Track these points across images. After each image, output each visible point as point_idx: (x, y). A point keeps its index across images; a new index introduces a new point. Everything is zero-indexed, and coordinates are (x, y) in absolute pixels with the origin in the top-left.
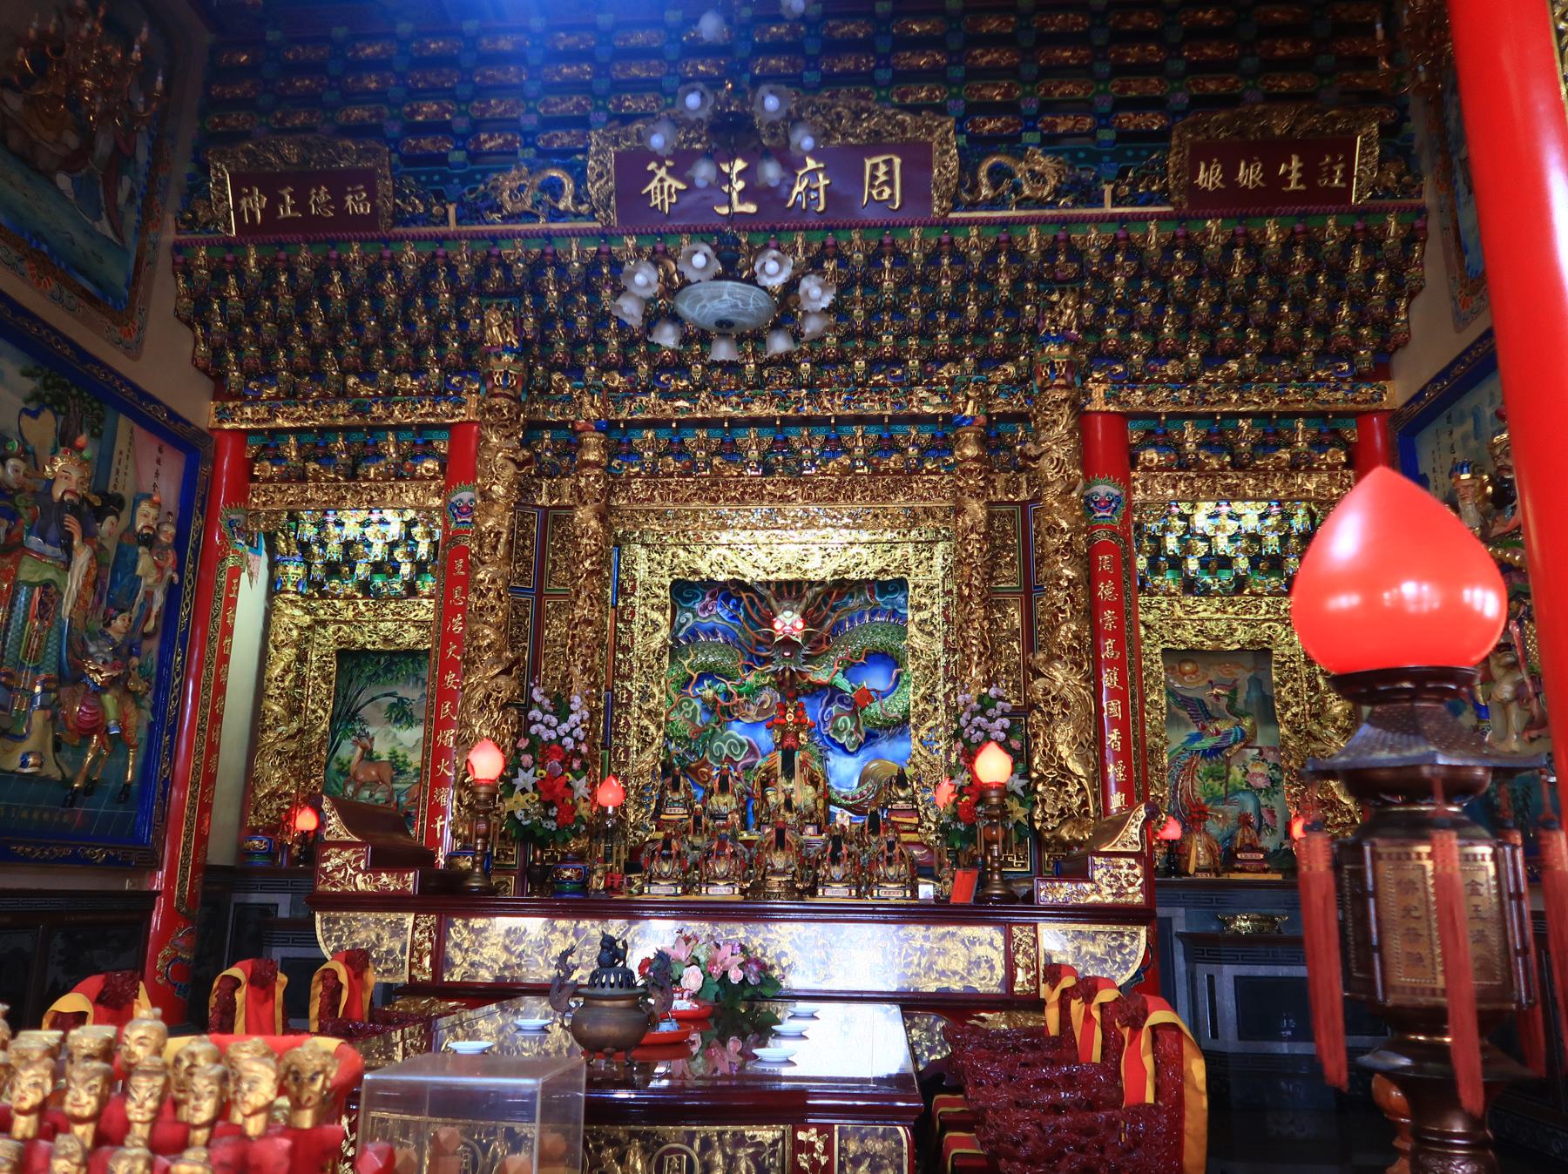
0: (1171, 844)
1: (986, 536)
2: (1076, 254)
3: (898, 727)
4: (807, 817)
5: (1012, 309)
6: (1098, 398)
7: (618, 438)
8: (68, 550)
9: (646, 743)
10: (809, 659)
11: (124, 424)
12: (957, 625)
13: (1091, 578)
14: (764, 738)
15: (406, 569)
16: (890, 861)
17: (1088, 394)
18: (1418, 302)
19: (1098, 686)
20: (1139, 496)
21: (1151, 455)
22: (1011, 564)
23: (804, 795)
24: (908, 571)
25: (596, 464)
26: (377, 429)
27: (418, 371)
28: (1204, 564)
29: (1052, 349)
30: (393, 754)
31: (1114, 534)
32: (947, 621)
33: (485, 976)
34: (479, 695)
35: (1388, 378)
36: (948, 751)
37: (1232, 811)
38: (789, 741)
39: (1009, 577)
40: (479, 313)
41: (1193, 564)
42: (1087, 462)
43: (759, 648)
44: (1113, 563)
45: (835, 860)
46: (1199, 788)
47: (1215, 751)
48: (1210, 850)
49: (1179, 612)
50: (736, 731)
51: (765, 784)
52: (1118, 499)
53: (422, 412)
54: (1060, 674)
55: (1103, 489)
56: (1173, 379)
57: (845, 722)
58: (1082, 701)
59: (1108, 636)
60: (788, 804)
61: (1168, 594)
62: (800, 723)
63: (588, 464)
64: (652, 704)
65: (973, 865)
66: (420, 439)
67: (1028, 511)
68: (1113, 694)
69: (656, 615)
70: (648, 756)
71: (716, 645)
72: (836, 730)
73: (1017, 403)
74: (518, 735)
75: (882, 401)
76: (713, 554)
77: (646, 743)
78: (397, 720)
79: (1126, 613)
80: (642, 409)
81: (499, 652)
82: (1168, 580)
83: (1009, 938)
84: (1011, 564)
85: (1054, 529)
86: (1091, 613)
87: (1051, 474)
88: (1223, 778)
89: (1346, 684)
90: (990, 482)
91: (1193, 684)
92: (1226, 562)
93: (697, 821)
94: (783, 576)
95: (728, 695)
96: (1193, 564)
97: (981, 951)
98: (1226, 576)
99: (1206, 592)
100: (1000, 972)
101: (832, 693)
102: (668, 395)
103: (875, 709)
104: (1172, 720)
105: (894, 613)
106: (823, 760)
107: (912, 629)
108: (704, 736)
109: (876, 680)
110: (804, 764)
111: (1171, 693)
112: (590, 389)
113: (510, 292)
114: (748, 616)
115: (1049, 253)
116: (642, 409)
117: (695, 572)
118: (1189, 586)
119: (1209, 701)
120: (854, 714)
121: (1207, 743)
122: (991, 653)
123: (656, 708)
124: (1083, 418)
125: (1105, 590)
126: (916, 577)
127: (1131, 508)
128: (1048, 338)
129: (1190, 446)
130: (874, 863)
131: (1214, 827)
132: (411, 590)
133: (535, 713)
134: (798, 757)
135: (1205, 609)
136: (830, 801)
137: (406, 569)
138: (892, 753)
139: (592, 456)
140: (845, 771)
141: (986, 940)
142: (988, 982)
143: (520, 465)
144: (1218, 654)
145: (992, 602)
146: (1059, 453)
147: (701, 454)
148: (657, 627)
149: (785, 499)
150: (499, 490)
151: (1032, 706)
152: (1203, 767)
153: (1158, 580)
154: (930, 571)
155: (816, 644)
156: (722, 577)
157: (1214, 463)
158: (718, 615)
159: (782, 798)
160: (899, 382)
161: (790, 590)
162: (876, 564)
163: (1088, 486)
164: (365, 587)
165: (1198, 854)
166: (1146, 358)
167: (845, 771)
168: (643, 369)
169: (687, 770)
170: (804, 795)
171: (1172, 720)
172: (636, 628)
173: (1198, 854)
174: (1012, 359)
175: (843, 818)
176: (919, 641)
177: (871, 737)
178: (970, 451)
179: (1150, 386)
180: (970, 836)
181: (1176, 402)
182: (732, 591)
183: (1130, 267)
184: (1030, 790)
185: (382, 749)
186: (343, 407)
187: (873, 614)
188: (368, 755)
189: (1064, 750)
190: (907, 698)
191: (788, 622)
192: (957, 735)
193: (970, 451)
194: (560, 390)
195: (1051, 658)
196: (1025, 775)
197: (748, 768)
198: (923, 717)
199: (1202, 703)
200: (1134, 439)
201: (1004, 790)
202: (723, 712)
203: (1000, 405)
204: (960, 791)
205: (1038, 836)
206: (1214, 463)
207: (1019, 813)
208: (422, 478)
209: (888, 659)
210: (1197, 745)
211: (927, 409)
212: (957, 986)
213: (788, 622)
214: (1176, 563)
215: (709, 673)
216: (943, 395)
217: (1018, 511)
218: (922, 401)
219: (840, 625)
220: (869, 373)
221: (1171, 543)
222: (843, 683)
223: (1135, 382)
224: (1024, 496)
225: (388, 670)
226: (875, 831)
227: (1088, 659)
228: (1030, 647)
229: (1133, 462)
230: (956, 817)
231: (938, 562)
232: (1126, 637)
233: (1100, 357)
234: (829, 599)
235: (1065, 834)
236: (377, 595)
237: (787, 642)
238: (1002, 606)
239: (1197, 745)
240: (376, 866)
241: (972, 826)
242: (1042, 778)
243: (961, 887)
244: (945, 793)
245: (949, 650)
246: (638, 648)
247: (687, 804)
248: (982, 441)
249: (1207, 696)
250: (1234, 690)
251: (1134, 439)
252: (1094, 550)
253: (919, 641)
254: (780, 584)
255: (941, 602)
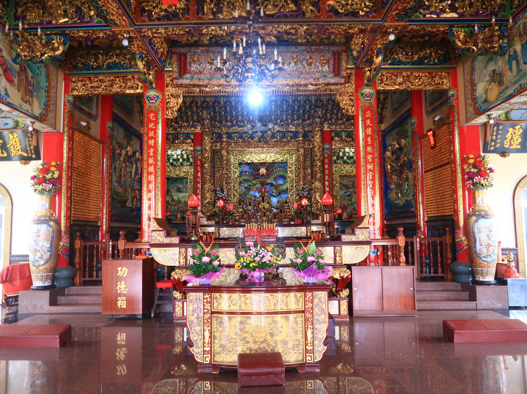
0: (339, 214)
1: (304, 156)
2: (321, 101)
3: (286, 191)
4: (268, 210)
5: (309, 111)
6: (326, 128)
7: (229, 136)
8: (132, 164)
9: (235, 196)
10: (267, 178)
11: (133, 136)
12: (298, 169)
13: (323, 164)
14: (258, 195)
15: (181, 160)
16: (285, 218)
17: (324, 127)
18: (387, 110)
19: (325, 185)
20: (333, 147)
21: (336, 138)
22: (308, 161)
23: (267, 206)
24: (288, 160)
25: (225, 142)
26: (179, 133)
27: (187, 121)
28: (347, 158)
29: (317, 119)
30: (178, 199)
31: (328, 155)
32: (296, 171)
33: (226, 237)
34: (207, 189)
35: (382, 123)
36: (296, 197)
37: (352, 207)
38: (263, 195)
39: (308, 163)
40: (202, 111)
41: (345, 158)
42: (323, 142)
43: (256, 175)
44: (328, 161)
45: (275, 218)
46: (346, 203)
47: (349, 195)
48: (347, 215)
49: (342, 168)
50: (251, 192)
51: (258, 204)
52: (329, 148)
53: (188, 130)
54: (317, 183)
55: (326, 146)
56: (341, 124)
57: (274, 191)
58: (321, 188)
59: (327, 173)
60: (264, 208)
61: (340, 164)
62: (265, 191)
63: (224, 141)
64: (236, 188)
65: (301, 218)
66: (187, 136)
67: (312, 150)
68: (328, 186)
69: (236, 170)
70: (235, 199)
71: (247, 175)
72: (273, 192)
73: (310, 129)
74: (215, 197)
75: (283, 128)
76: (247, 157)
77: (235, 196)
78: (178, 192)
79: (330, 169)
80: (234, 130)
81: (210, 181)
82: (340, 161)
83: (307, 229)
84: (308, 161)
85: (316, 156)
86: (323, 172)
87: (316, 144)
88: (351, 200)
89: (324, 206)
90: (304, 144)
91: (345, 182)
92: (352, 157)
93: (245, 211)
94: (262, 161)
95: (250, 185)
96: (345, 158)
97: (303, 230)
98: (352, 160)
99: (348, 163)
100: (305, 233)
101: (272, 185)
102: (240, 127)
103: (281, 188)
104: (341, 189)
105: (284, 167)
106: (270, 198)
107: (289, 172)
108: (245, 194)
109: (281, 182)
110: (266, 200)
111: (341, 183)
112: (224, 126)
113: (207, 108)
114: (253, 169)
115: (316, 101)
116: (234, 130)
117: (244, 161)
118: (345, 162)
119: (349, 185)
120: (276, 189)
121: (348, 194)
122: (304, 178)
123: (235, 190)
124: (322, 131)
125: (326, 166)
126: (290, 161)
127: (332, 149)
128: (316, 117)
129: (344, 137)
130: (282, 219)
131: (349, 210)
132: (182, 164)
133: (218, 192)
134: (265, 198)
135: (348, 167)
136: (272, 207)
137: (181, 160)
138: (284, 196)
139: (225, 140)
140: (274, 200)
141: (304, 229)
142: (304, 235)
143: (212, 143)
144: (350, 176)
145: (305, 168)
146: (318, 140)
147: (246, 138)
148: (236, 173)
149: (263, 147)
150: (207, 148)
151: (311, 189)
152: (347, 198)
153: (338, 161)
154: (292, 160)
155: (268, 175)
156: (249, 162)
157: (349, 140)
158: (247, 168)
159: (262, 207)
160: (286, 124)
161: (263, 164)
162: (281, 159)
163: (323, 145)
164: (172, 164)
165: (345, 216)
166: (335, 120)
167: (274, 200)
168: (235, 122)
169: (243, 201)
170: (267, 206)
171: (341, 189)
172: (232, 172)
173: (345, 216)
174: (309, 120)
175: (275, 211)
176: (290, 175)
177: (280, 194)
178: (301, 139)
179: (337, 124)
180: (301, 213)
181: (341, 128)
182: (251, 164)
183: (332, 103)
184: (311, 205)
185: (176, 198)
186: (171, 129)
187: (280, 168)
188: (173, 199)
189: (317, 197)
190: (288, 185)
191: (263, 171)
192: (298, 194)
193: (301, 139)
194: (217, 125)
195: (316, 180)
196: (311, 202)
197: (254, 200)
198: (291, 190)
199: (347, 185)
200: (333, 135)
201: (307, 206)
202: (248, 189)
203: (306, 129)
204: (299, 205)
205: (313, 213)
206: (349, 140)
207: (309, 209)
208: (188, 143)
209: (284, 177)
210: (346, 194)
211: (293, 130)
212: (299, 236)
213: (263, 171)
214: (342, 158)
215: (246, 181)
216: (295, 127)
217: (310, 150)
218: (291, 128)
219: (273, 170)
220: (280, 123)
221: (341, 154)
222: (274, 183)
223: (333, 125)
224: (311, 147)
225: (175, 181)
226: (281, 213)
227: (322, 180)
228: (312, 178)
229: (333, 139)
230: (298, 210)
231: (294, 158)
232: (331, 174)
233: (326, 120)
234: (270, 166)
235: (317, 213)
236: (175, 166)
237: (263, 175)
238: (306, 169)
239: (346, 194)
240: (208, 220)
241: (301, 212)
242: (313, 203)
243: (299, 221)
244: (296, 205)
245: (296, 176)
246: (232, 177)
247: (243, 208)
248: (303, 137)
249: (348, 184)
250: (354, 183)
251: (333, 135)
252: (324, 158)
253: (290, 175)
254: (261, 163)
255: (294, 167)
